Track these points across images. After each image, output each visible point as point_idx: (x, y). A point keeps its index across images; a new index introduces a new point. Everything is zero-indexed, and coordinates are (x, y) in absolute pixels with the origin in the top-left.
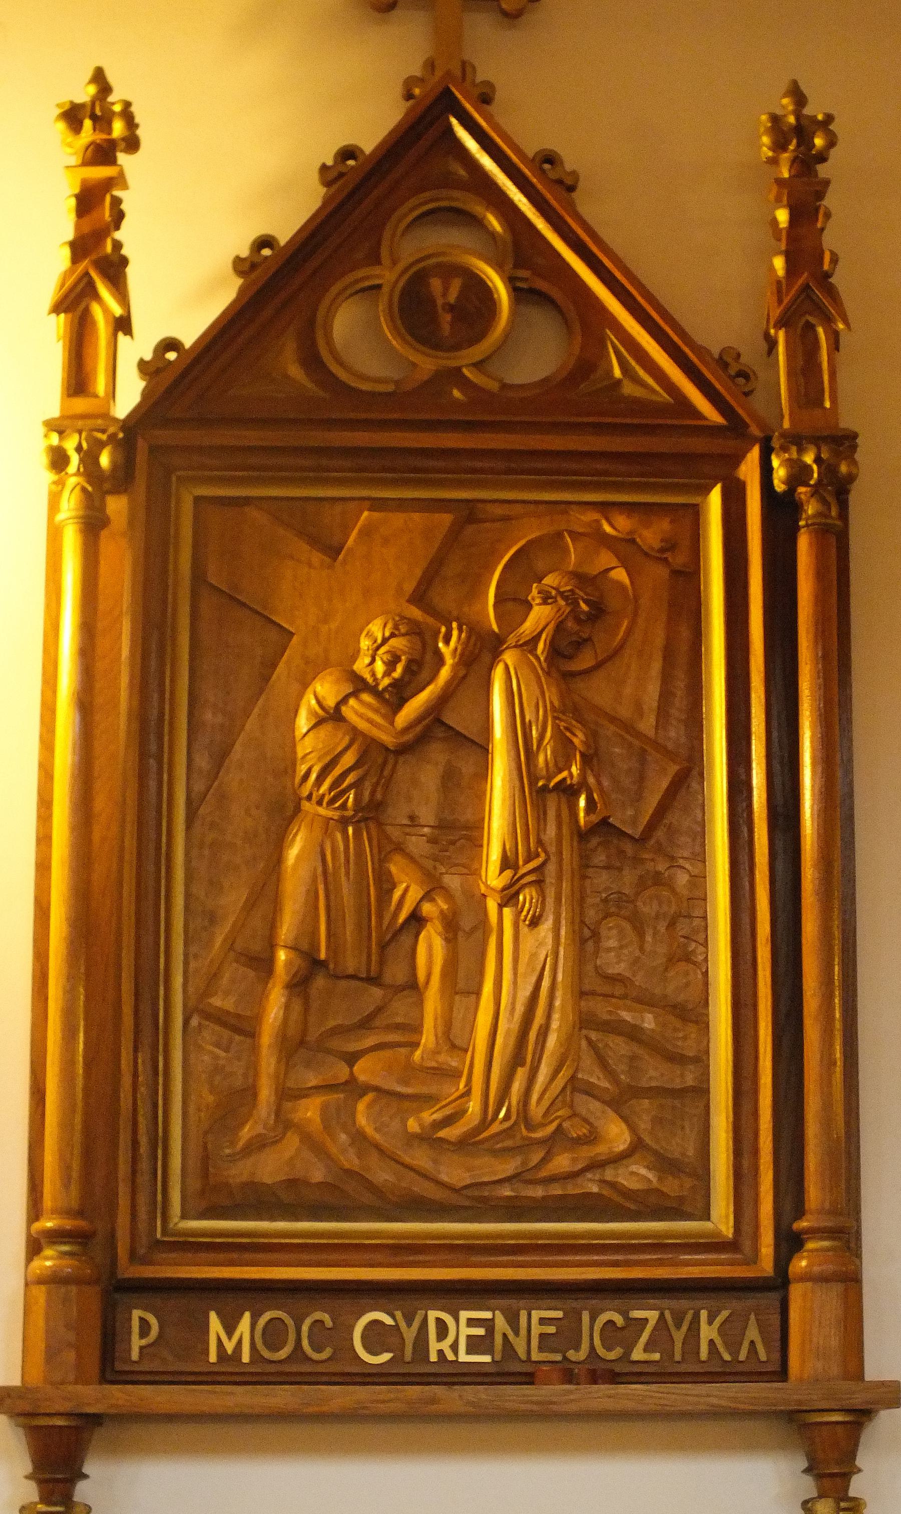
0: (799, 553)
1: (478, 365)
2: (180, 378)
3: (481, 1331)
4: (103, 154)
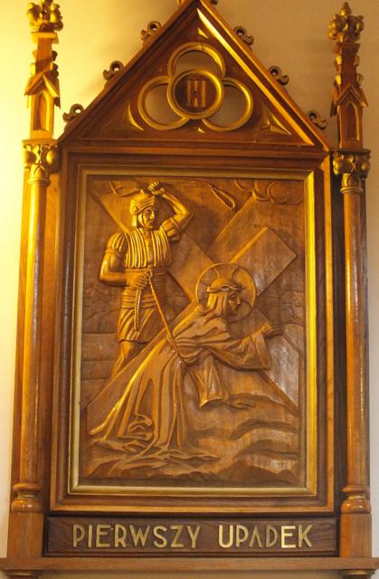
2: (81, 122)
3: (291, 535)
4: (48, 28)
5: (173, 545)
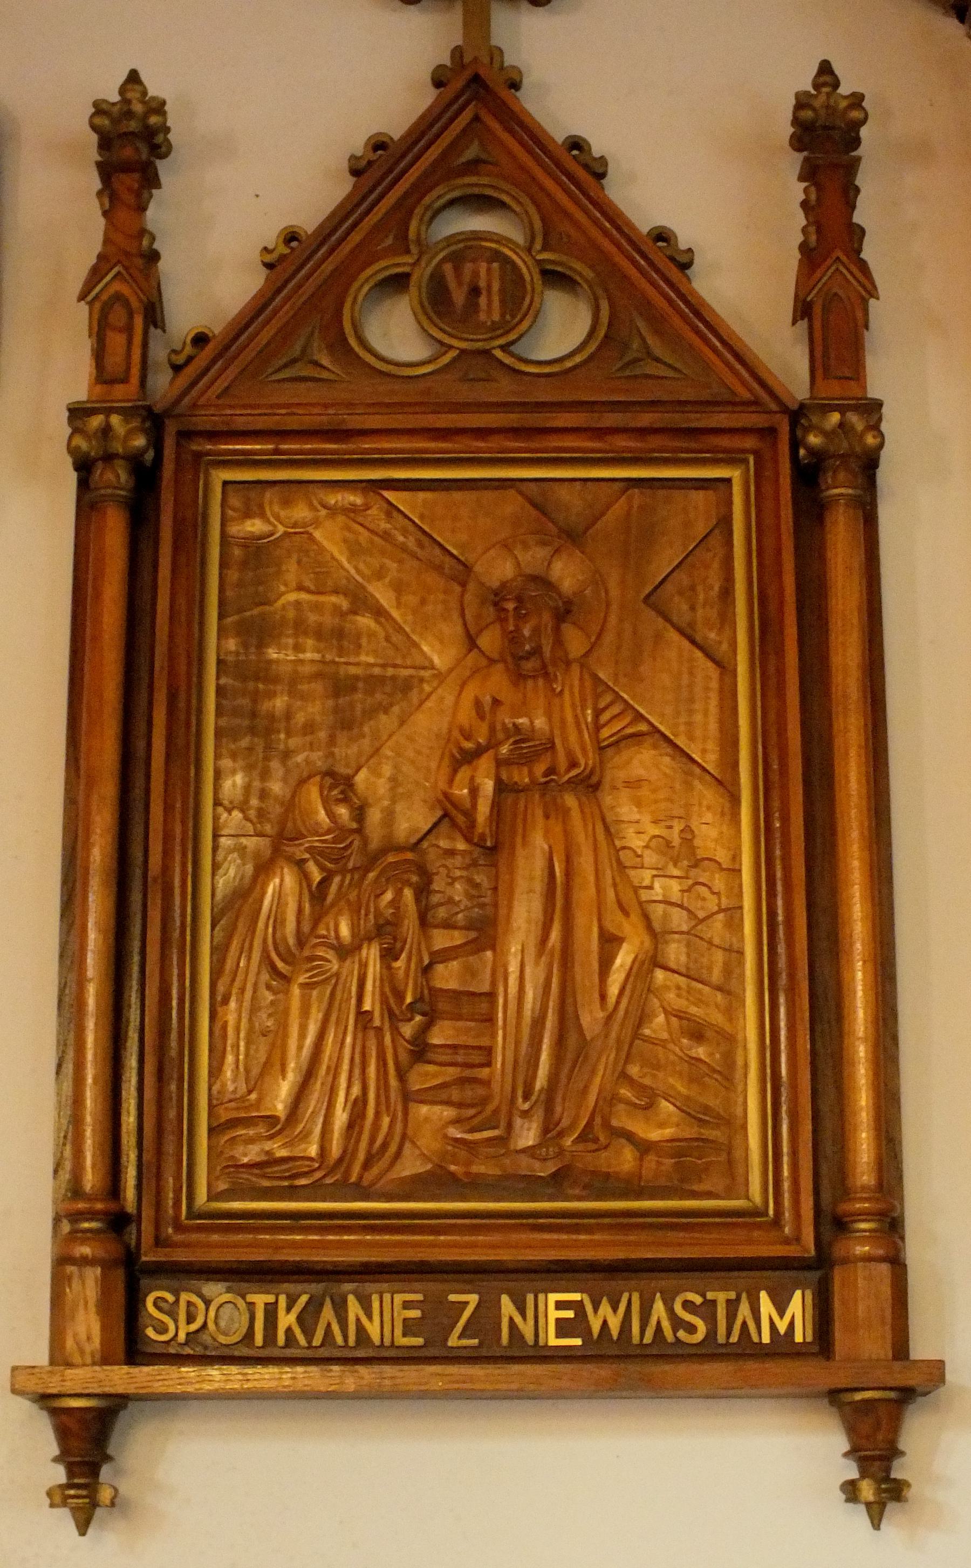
0: (734, 522)
1: (503, 348)
3: (570, 1314)
5: (473, 1299)
